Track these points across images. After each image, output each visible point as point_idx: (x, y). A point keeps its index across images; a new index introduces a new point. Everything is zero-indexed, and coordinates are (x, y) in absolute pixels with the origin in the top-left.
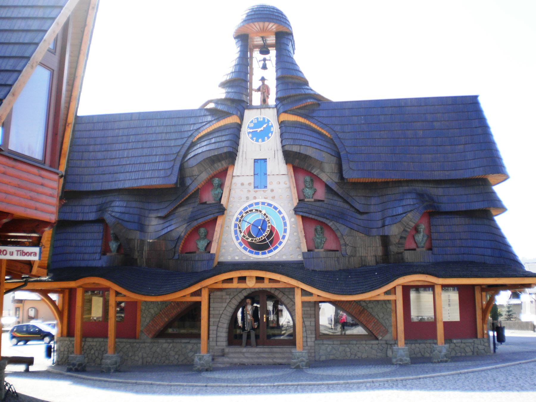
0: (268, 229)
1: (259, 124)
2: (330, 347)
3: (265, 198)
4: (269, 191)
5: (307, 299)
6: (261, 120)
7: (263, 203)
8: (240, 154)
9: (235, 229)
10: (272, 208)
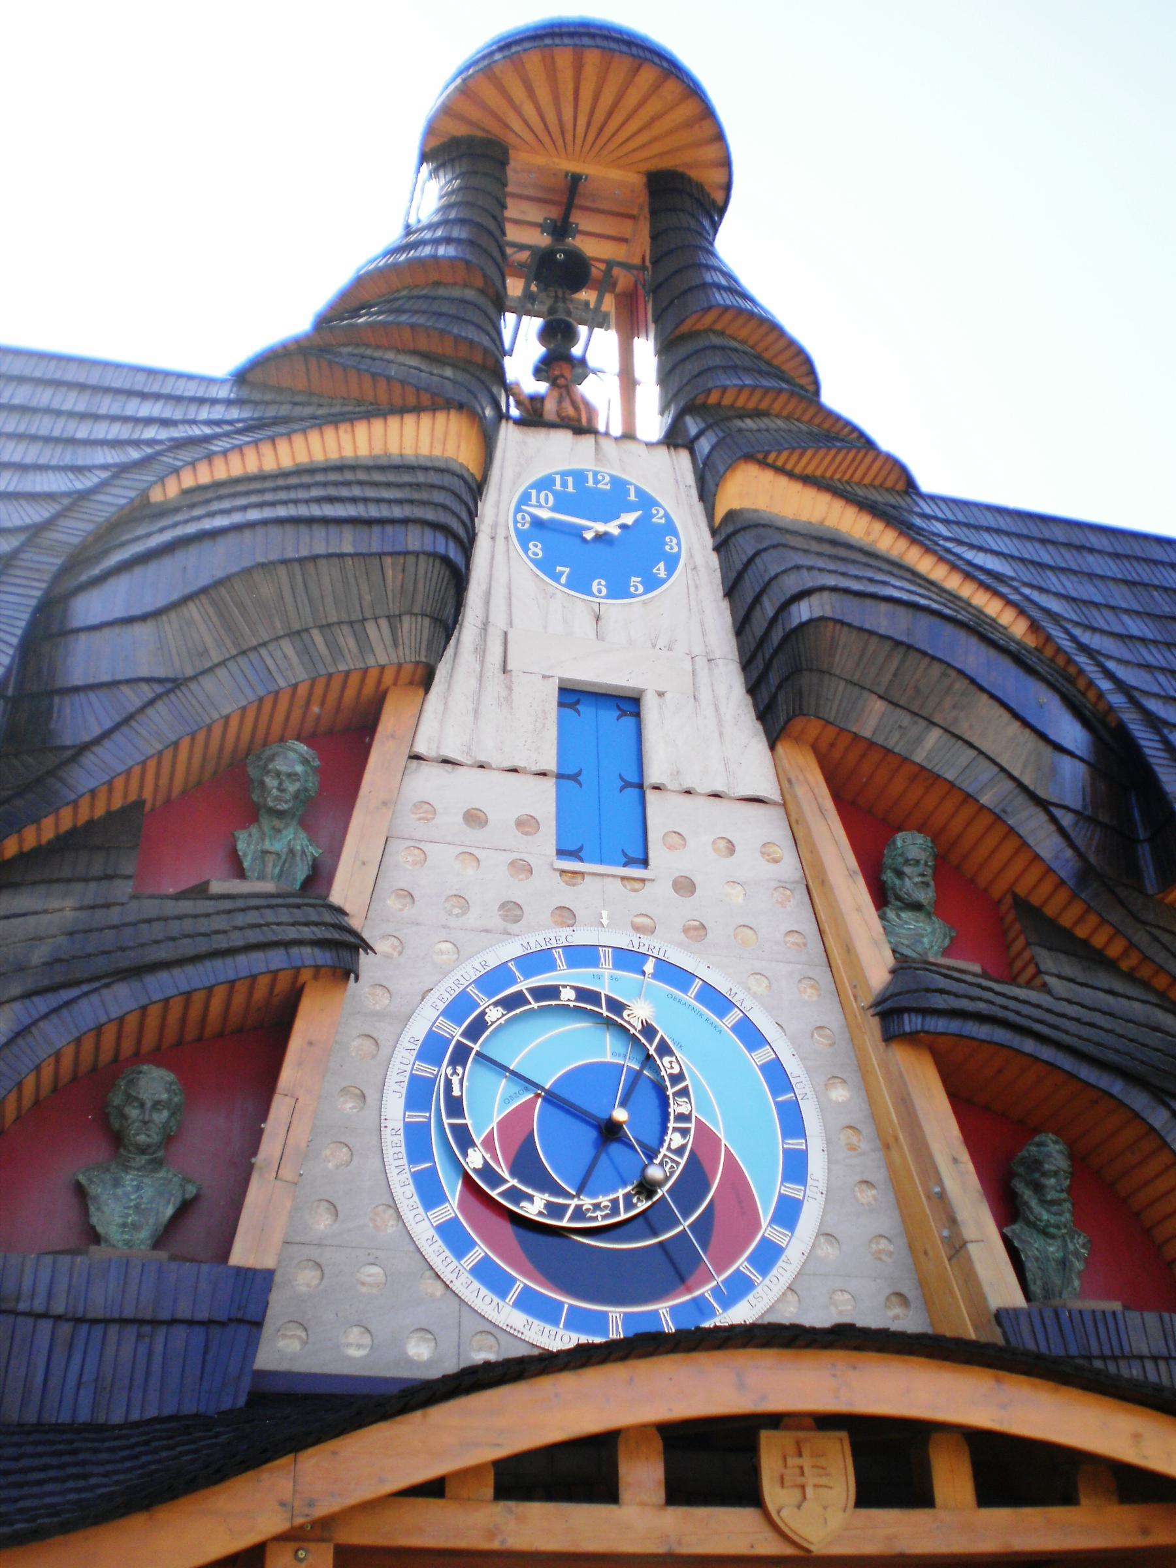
0: (676, 1140)
7: (629, 959)
9: (419, 1117)
10: (689, 997)
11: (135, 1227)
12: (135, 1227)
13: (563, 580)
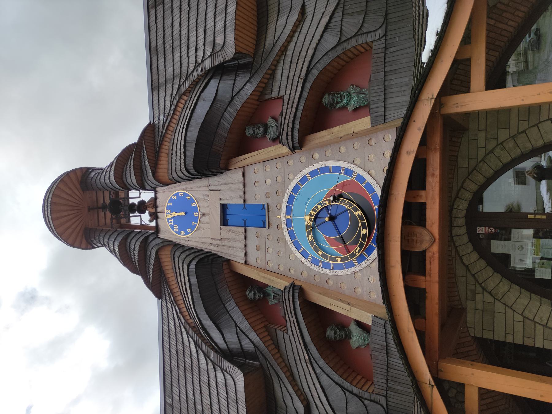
5: (478, 75)
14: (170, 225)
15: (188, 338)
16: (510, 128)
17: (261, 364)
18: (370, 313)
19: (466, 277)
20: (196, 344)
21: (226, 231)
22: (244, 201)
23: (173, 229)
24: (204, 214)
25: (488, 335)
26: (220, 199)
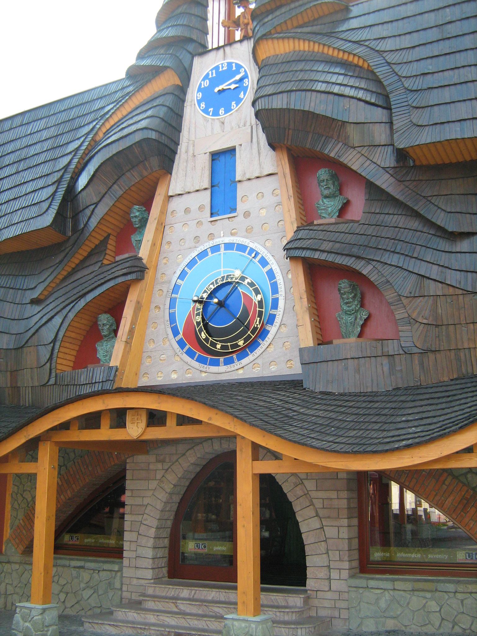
1: (222, 75)
2: (387, 595)
3: (232, 234)
4: (241, 218)
6: (225, 68)
8: (182, 149)
11: (106, 356)
12: (106, 356)
13: (211, 114)
14: (208, 74)
15: (83, 136)
16: (316, 490)
17: (69, 237)
18: (120, 364)
19: (176, 454)
20: (77, 149)
21: (204, 161)
22: (240, 181)
23: (204, 80)
24: (223, 123)
25: (129, 475)
26: (241, 145)
